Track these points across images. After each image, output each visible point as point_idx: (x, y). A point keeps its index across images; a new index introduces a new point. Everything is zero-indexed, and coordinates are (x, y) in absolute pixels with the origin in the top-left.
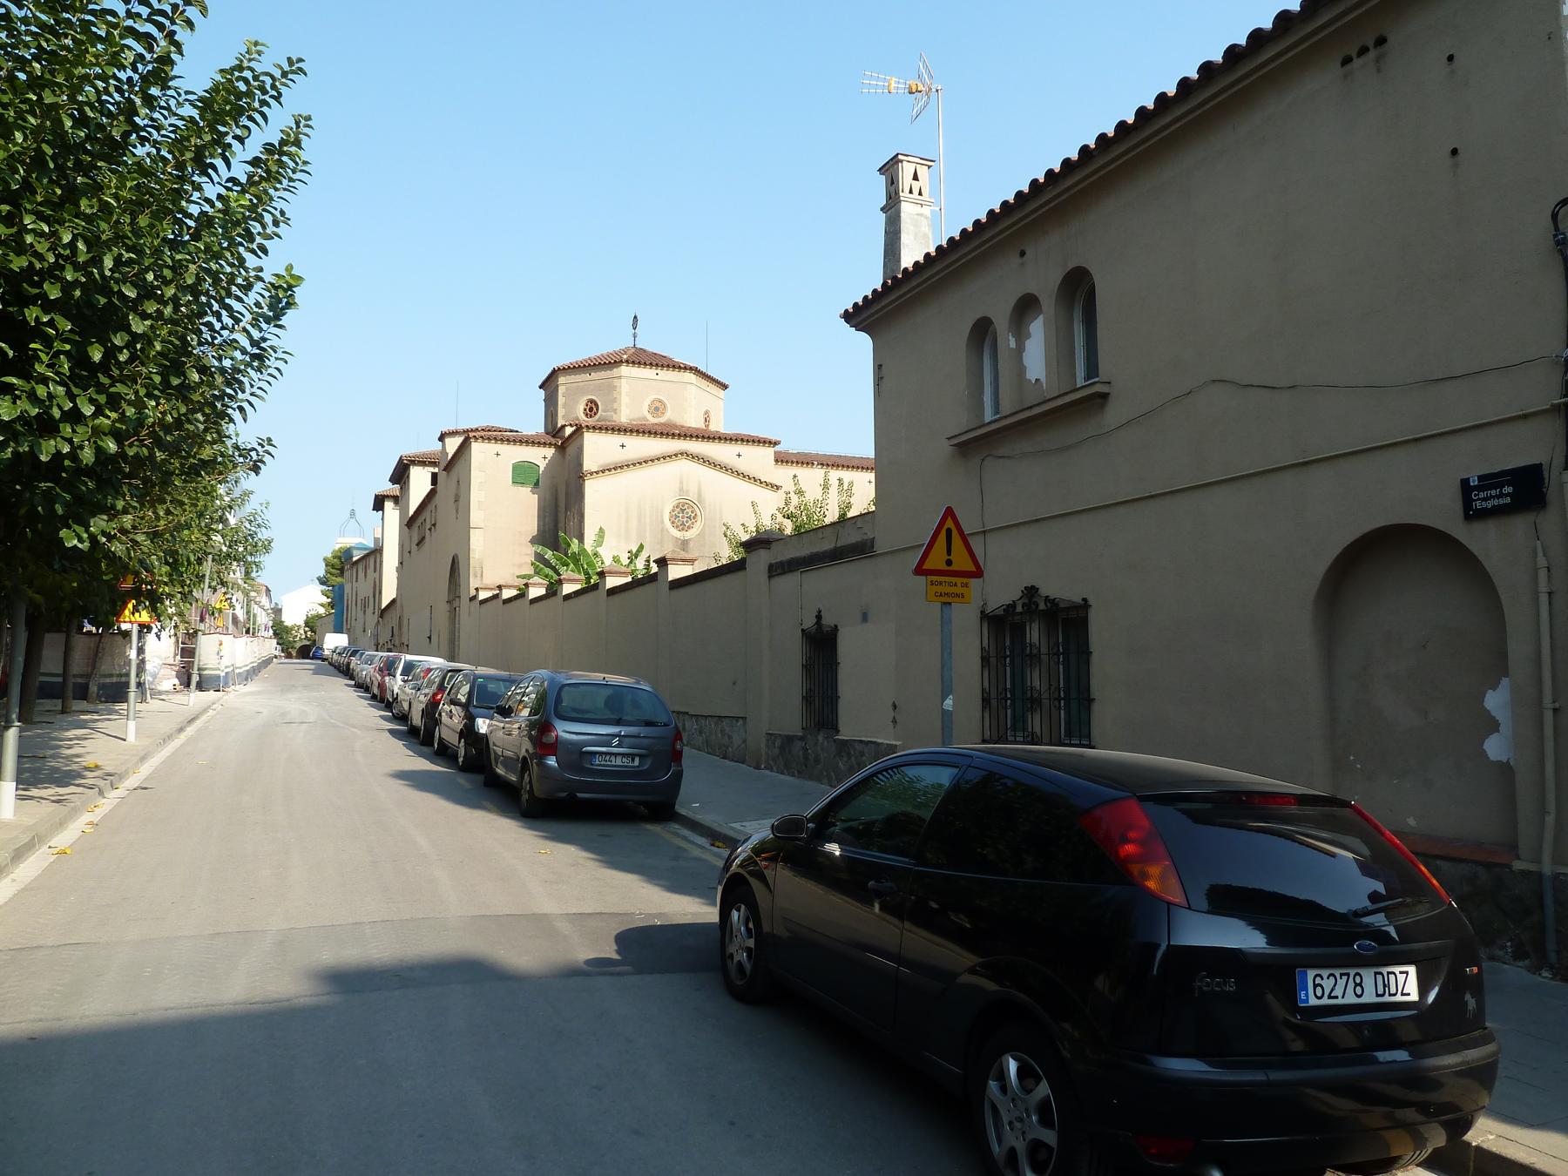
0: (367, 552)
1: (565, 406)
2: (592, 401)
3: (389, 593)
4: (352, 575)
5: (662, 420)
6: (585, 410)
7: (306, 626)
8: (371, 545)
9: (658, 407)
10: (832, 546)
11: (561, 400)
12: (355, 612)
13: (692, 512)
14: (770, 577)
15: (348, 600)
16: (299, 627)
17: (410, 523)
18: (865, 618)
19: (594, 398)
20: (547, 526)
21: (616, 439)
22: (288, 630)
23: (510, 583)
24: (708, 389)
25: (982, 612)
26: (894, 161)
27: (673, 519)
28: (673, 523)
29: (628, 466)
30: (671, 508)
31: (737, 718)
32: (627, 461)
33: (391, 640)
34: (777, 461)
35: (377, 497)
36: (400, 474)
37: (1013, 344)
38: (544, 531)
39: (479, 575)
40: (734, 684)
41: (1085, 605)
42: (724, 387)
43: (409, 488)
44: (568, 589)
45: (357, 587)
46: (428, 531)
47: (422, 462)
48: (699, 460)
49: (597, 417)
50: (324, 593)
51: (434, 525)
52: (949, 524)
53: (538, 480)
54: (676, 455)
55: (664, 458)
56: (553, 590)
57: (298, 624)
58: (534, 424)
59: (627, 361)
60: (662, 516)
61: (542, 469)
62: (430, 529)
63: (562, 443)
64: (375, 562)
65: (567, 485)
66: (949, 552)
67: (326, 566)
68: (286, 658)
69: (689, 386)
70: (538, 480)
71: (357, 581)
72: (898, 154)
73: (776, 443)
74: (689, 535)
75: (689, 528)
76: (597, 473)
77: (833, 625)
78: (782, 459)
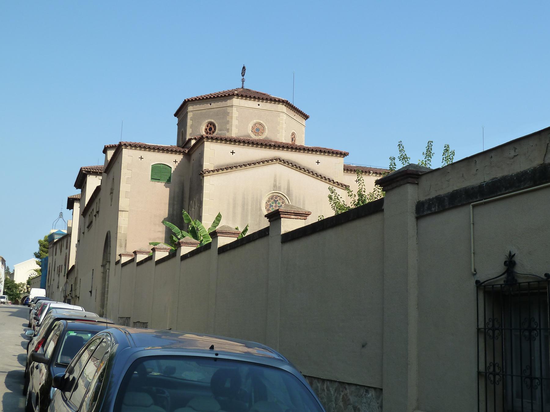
1: (192, 126)
2: (211, 123)
3: (72, 262)
4: (53, 251)
6: (206, 129)
7: (28, 284)
8: (65, 232)
9: (258, 128)
10: (541, 162)
11: (189, 122)
12: (54, 275)
14: (418, 218)
15: (50, 267)
16: (24, 284)
17: (84, 213)
19: (213, 121)
20: (175, 212)
21: (228, 148)
22: (16, 286)
23: (143, 250)
24: (295, 118)
29: (236, 167)
31: (367, 388)
32: (235, 164)
33: (70, 294)
34: (344, 170)
35: (69, 199)
36: (81, 183)
38: (173, 215)
39: (123, 246)
40: (363, 346)
42: (306, 117)
43: (86, 190)
44: (185, 250)
45: (57, 259)
46: (94, 217)
47: (95, 172)
48: (288, 164)
50: (37, 263)
51: (98, 212)
53: (170, 178)
54: (272, 160)
55: (263, 162)
56: (173, 255)
57: (23, 283)
58: (172, 141)
59: (237, 95)
61: (173, 169)
62: (95, 216)
63: (188, 151)
64: (67, 242)
65: (191, 182)
67: (40, 246)
68: (14, 304)
69: (281, 114)
70: (170, 178)
71: (56, 255)
73: (344, 155)
76: (213, 171)
78: (348, 169)
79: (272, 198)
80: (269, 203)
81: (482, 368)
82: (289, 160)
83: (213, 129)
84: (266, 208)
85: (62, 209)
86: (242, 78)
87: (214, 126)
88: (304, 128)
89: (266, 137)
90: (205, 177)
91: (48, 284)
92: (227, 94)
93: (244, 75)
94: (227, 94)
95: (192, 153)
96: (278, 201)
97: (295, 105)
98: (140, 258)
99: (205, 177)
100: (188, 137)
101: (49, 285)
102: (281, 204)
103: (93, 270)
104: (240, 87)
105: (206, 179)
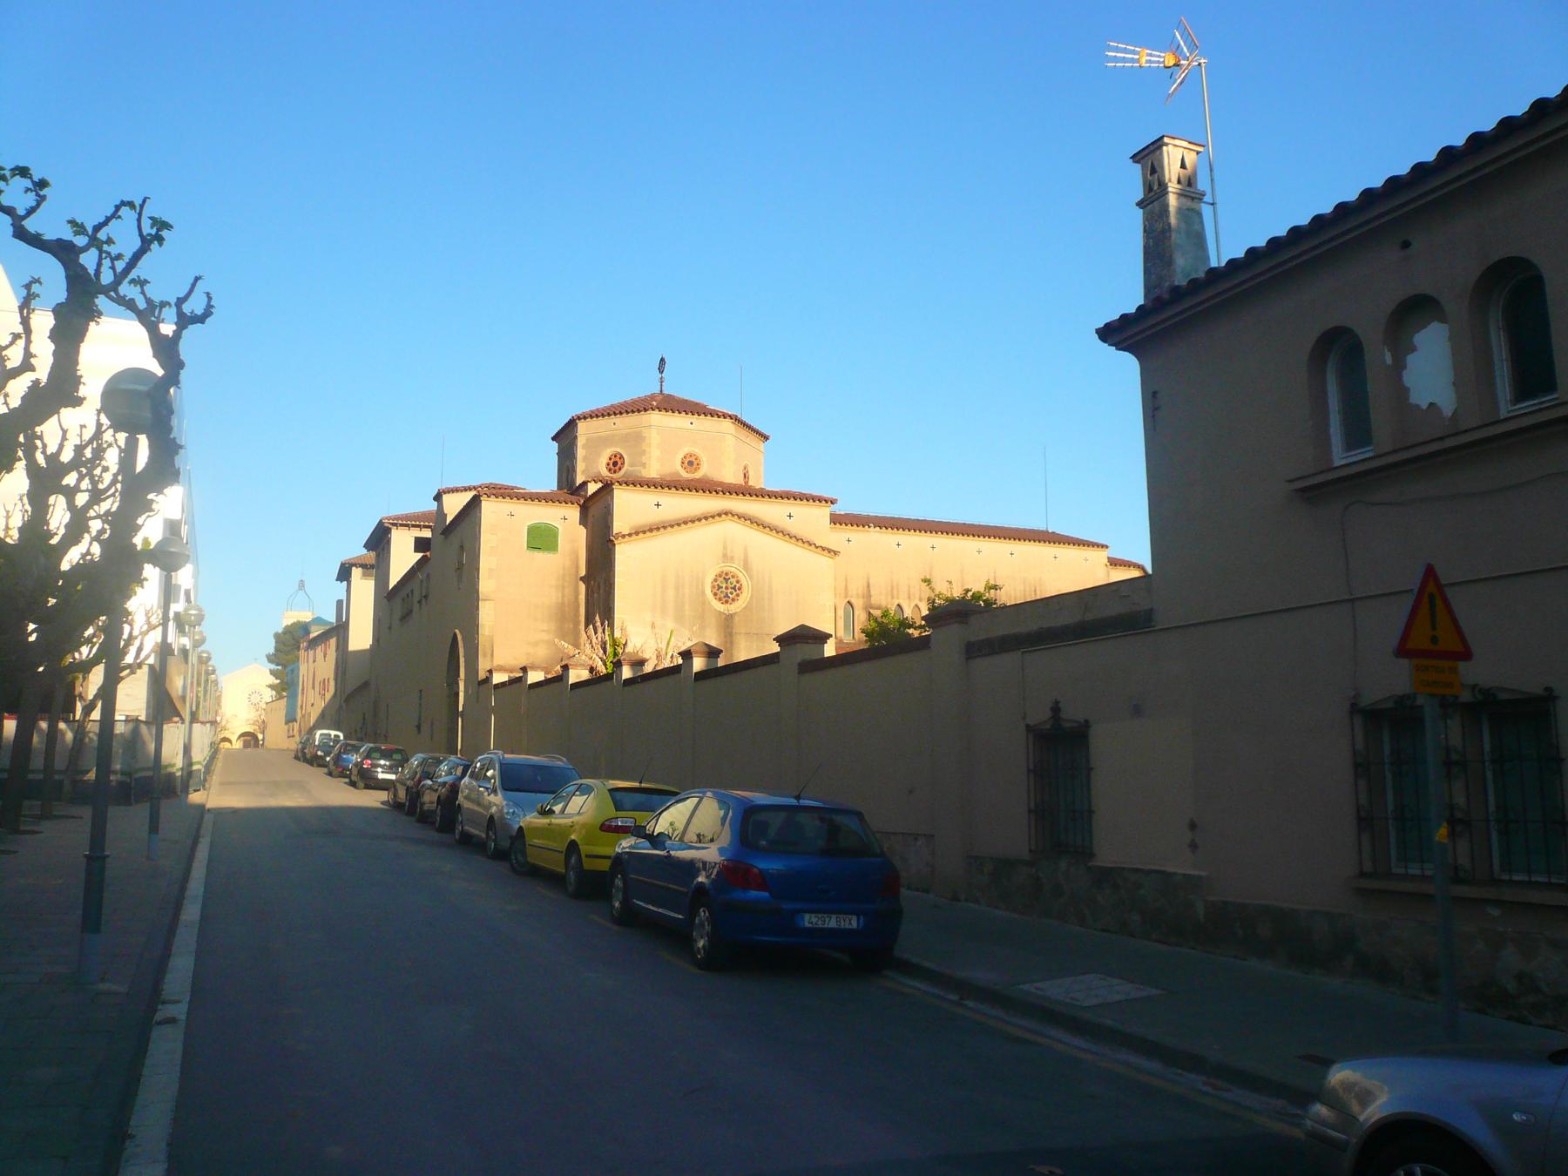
0: (327, 628)
1: (585, 459)
5: (698, 475)
6: (608, 464)
9: (691, 462)
11: (581, 453)
13: (738, 582)
18: (1137, 711)
20: (566, 599)
25: (1353, 705)
26: (1159, 143)
27: (715, 590)
28: (715, 594)
30: (713, 576)
31: (916, 837)
35: (343, 565)
36: (379, 540)
37: (1389, 359)
39: (489, 656)
40: (911, 792)
41: (1549, 697)
49: (623, 472)
50: (272, 673)
51: (426, 597)
52: (1431, 587)
54: (719, 515)
60: (703, 586)
62: (420, 602)
66: (1434, 628)
71: (314, 661)
72: (1163, 137)
74: (733, 608)
75: (733, 600)
76: (630, 535)
77: (1082, 721)
78: (836, 520)
81: (1032, 806)
83: (619, 463)
90: (617, 547)
97: (744, 419)
98: (534, 677)
104: (657, 391)
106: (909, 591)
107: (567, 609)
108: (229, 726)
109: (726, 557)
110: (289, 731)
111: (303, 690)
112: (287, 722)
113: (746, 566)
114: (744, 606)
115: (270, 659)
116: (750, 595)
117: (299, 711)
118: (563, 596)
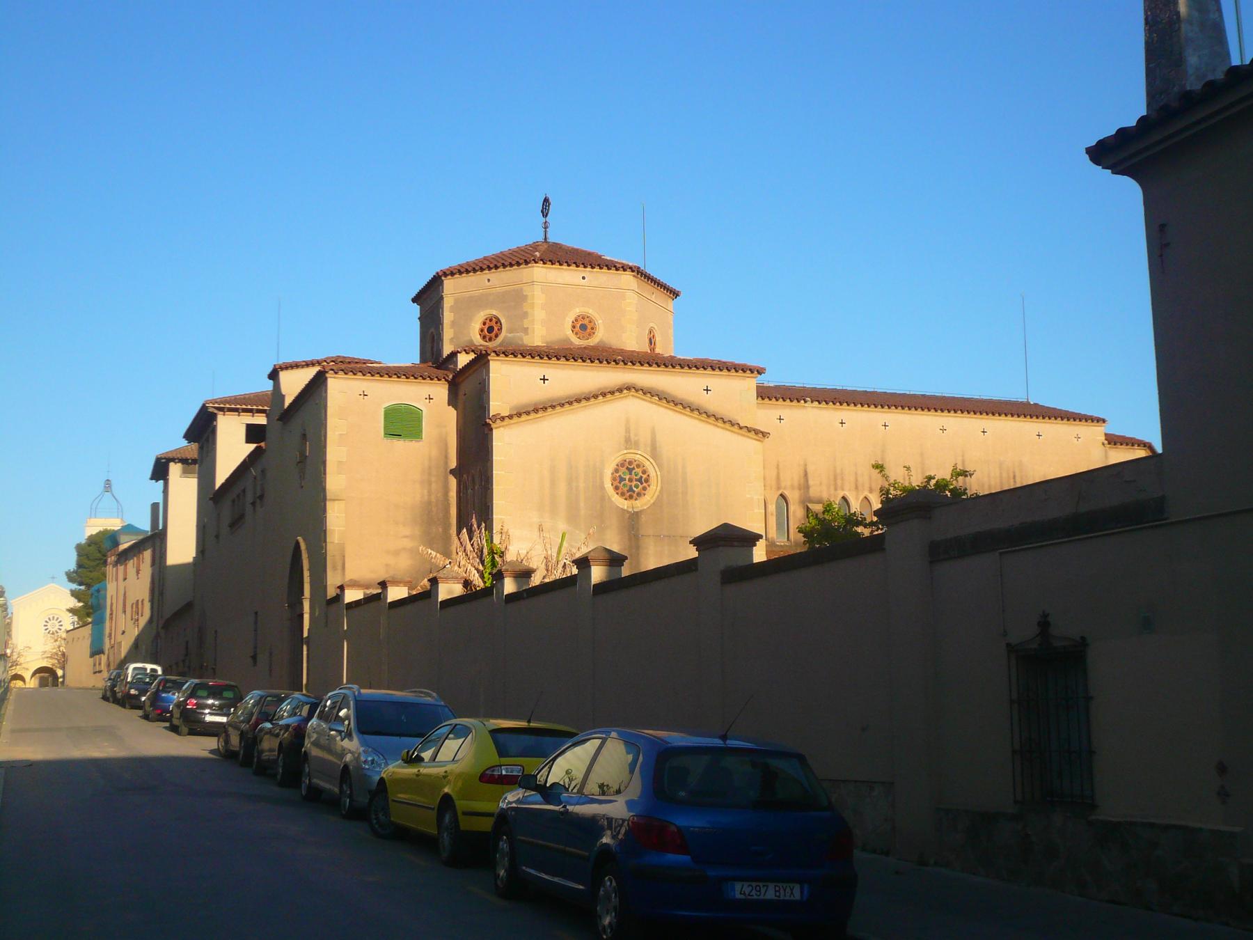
0: (141, 537)
1: (453, 324)
5: (593, 341)
6: (482, 330)
9: (584, 326)
11: (448, 317)
14: (931, 562)
20: (433, 499)
27: (616, 483)
28: (616, 488)
33: (184, 661)
39: (339, 568)
50: (74, 594)
51: (261, 497)
54: (620, 390)
62: (253, 504)
73: (760, 371)
74: (639, 504)
75: (639, 494)
76: (510, 417)
78: (764, 394)
79: (622, 465)
80: (617, 475)
82: (652, 388)
83: (496, 328)
84: (612, 485)
85: (108, 472)
86: (544, 220)
87: (498, 321)
88: (671, 317)
89: (601, 341)
91: (110, 642)
92: (521, 259)
93: (546, 216)
94: (521, 259)
95: (462, 381)
96: (634, 468)
99: (494, 430)
100: (447, 350)
101: (113, 642)
102: (641, 474)
103: (256, 613)
104: (541, 238)
105: (496, 434)
106: (857, 480)
107: (434, 509)
108: (21, 660)
109: (629, 442)
110: (95, 665)
111: (111, 614)
112: (93, 655)
113: (655, 453)
114: (652, 501)
115: (71, 577)
116: (659, 488)
117: (107, 640)
118: (430, 493)
